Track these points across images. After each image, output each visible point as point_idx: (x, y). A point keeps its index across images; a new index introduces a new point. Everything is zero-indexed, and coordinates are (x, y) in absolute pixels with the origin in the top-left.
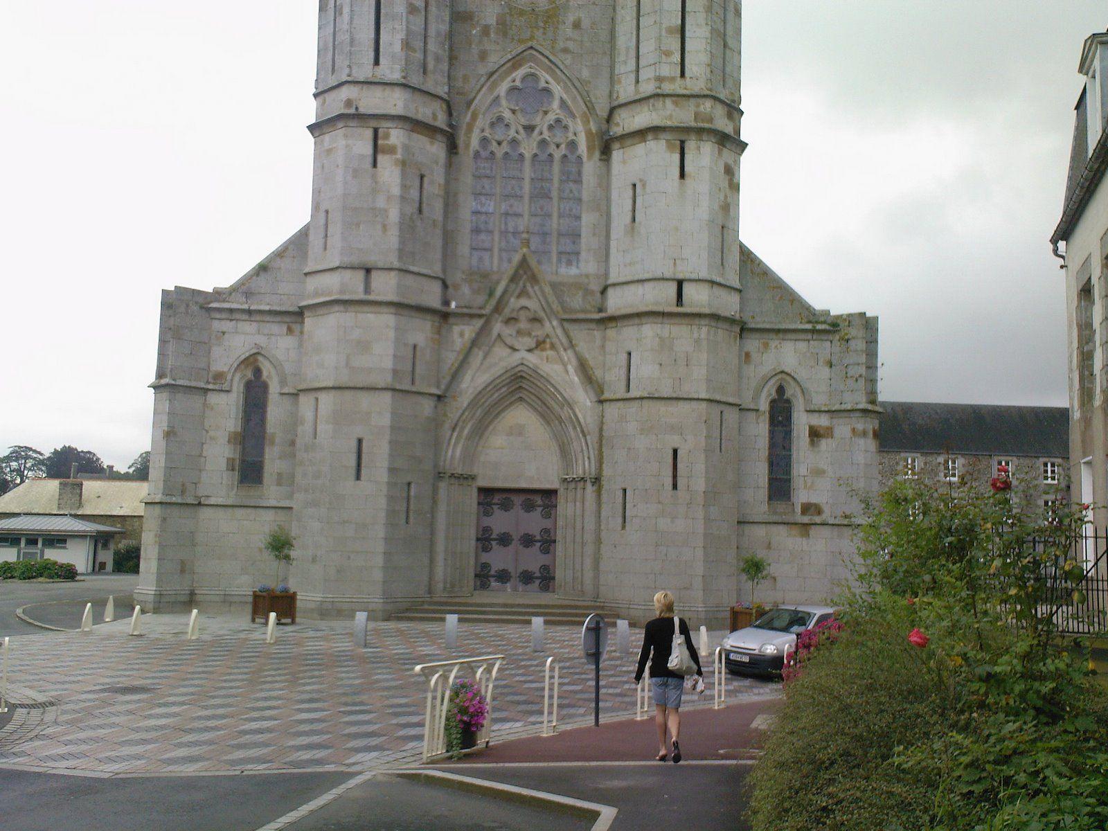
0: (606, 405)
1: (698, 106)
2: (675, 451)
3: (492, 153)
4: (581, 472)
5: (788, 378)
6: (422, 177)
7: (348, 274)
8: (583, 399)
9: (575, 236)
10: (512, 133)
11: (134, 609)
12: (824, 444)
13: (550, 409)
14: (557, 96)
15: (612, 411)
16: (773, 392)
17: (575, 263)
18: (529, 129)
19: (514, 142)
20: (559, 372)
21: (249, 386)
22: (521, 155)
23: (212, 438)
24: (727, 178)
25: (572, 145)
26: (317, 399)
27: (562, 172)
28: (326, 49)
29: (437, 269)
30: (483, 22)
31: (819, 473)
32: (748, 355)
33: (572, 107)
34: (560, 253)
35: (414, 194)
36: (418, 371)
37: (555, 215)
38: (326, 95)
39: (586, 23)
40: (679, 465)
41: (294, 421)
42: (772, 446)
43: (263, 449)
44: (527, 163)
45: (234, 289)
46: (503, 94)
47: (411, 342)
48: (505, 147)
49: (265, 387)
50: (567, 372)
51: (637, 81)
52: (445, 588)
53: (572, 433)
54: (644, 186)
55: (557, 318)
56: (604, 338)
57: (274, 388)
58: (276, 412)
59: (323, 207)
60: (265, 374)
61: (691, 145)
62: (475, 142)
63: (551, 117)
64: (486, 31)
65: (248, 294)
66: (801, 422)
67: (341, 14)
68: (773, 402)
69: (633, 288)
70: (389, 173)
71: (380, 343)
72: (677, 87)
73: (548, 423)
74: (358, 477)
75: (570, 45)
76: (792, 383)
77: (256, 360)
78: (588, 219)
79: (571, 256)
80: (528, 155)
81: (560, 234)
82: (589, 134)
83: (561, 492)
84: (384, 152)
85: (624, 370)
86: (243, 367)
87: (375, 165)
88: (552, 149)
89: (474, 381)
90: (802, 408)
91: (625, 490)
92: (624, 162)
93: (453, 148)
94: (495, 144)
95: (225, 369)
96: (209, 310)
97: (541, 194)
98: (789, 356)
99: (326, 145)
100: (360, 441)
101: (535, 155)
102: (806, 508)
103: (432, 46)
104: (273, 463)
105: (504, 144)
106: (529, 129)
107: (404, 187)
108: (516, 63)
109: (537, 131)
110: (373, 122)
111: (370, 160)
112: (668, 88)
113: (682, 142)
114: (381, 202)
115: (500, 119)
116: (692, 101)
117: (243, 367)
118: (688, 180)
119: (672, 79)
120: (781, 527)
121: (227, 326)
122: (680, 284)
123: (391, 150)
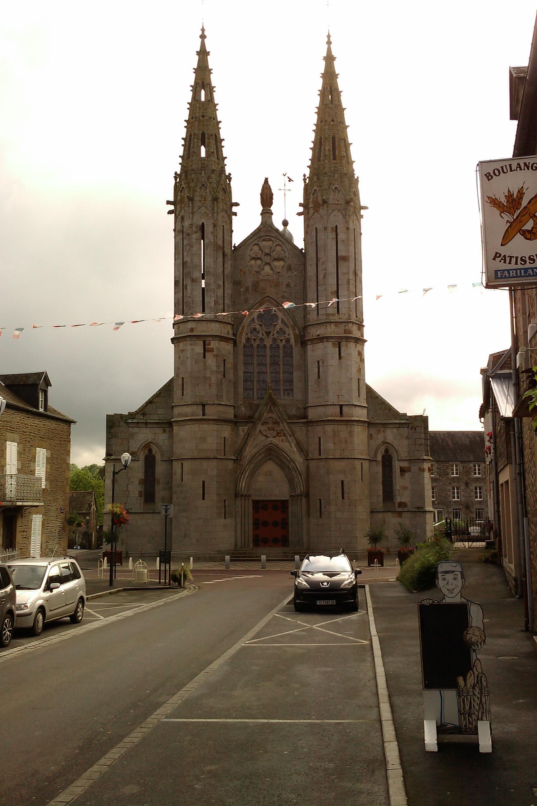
0: (310, 461)
1: (345, 326)
2: (342, 482)
3: (251, 344)
4: (299, 492)
5: (390, 446)
6: (224, 360)
7: (195, 407)
8: (298, 459)
9: (291, 381)
10: (260, 335)
11: (190, 560)
12: (407, 475)
13: (283, 462)
14: (280, 318)
15: (312, 464)
16: (383, 451)
17: (291, 395)
18: (268, 333)
19: (262, 340)
20: (289, 447)
21: (146, 457)
22: (265, 345)
23: (132, 482)
24: (359, 357)
25: (288, 341)
26: (182, 464)
27: (284, 353)
28: (178, 300)
29: (232, 403)
30: (246, 285)
31: (405, 488)
32: (371, 435)
33: (287, 323)
34: (284, 390)
35: (222, 369)
36: (226, 449)
37: (281, 372)
38: (180, 325)
39: (292, 285)
40: (345, 488)
41: (170, 474)
42: (384, 476)
43: (154, 486)
44: (268, 349)
45: (137, 413)
46: (256, 317)
47: (223, 436)
48: (258, 342)
49: (154, 458)
50: (291, 446)
51: (318, 314)
52: (241, 547)
53: (294, 473)
54: (323, 362)
55: (286, 422)
56: (307, 431)
57: (158, 457)
58: (160, 469)
59: (181, 376)
60: (154, 452)
61: (343, 344)
62: (244, 340)
63: (278, 328)
64: (247, 289)
65: (144, 415)
66: (397, 465)
67: (186, 288)
68: (383, 457)
69: (320, 408)
70: (211, 360)
71: (213, 437)
72: (336, 318)
73: (283, 470)
74: (204, 499)
75: (285, 294)
76: (392, 448)
77: (150, 445)
78: (296, 375)
79: (290, 391)
80: (268, 345)
81: (284, 381)
82: (295, 335)
83: (290, 501)
84: (208, 351)
85: (317, 446)
86: (144, 449)
87: (204, 357)
88: (279, 342)
89: (249, 451)
90: (396, 459)
91: (320, 500)
92: (313, 351)
93: (235, 344)
94: (252, 340)
95: (136, 450)
96: (127, 423)
97: (275, 363)
98: (390, 435)
99: (181, 348)
100: (204, 482)
101: (271, 345)
102: (401, 504)
103: (226, 301)
104: (160, 492)
105: (257, 340)
106: (268, 333)
107: (218, 366)
108: (261, 304)
109: (271, 334)
110: (204, 339)
111: (203, 355)
112: (332, 319)
113: (339, 343)
114: (208, 374)
115: (255, 329)
116: (343, 324)
117: (144, 449)
118: (342, 360)
119: (333, 315)
120: (389, 513)
121: (136, 430)
122: (341, 406)
123: (212, 350)
